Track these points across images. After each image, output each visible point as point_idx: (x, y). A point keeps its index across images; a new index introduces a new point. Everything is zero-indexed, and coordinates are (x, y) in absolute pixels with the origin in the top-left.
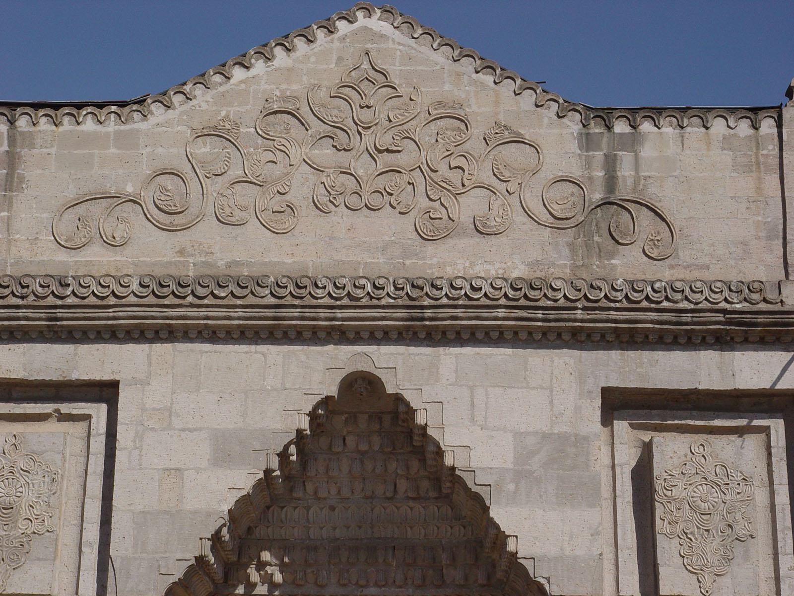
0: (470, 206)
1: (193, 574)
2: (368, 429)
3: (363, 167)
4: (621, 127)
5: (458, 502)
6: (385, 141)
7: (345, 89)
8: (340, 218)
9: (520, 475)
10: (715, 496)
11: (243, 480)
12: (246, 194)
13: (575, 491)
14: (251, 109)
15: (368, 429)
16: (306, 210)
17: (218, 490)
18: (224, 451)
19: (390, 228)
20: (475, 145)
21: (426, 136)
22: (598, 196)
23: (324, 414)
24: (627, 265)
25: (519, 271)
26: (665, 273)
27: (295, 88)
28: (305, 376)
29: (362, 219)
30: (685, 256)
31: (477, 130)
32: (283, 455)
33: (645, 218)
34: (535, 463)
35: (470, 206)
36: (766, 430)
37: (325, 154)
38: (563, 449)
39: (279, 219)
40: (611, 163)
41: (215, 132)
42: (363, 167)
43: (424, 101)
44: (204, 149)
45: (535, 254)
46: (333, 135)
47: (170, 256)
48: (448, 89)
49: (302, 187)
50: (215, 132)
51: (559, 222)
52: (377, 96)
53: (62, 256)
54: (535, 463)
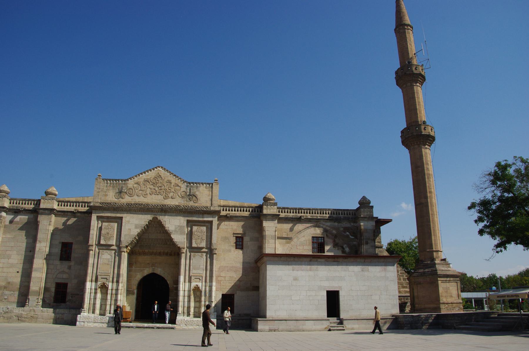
0: (171, 194)
1: (208, 284)
2: (156, 226)
3: (157, 189)
4: (192, 185)
5: (167, 234)
6: (160, 185)
7: (155, 178)
8: (153, 196)
9: (175, 231)
10: (200, 234)
11: (139, 230)
12: (140, 192)
13: (182, 233)
14: (142, 180)
15: (156, 226)
16: (149, 194)
17: (135, 232)
18: (136, 227)
19: (160, 197)
20: (172, 186)
21: (165, 185)
22: (188, 194)
23: (150, 222)
24: (191, 204)
25: (177, 204)
26: (196, 205)
27: (149, 177)
28: (149, 217)
29: (156, 196)
30: (199, 202)
31: (172, 184)
32: (144, 227)
33: (194, 198)
34: (177, 229)
35: (171, 194)
36: (211, 222)
37: (152, 187)
38: (181, 227)
39: (145, 196)
40: (190, 190)
41: (137, 183)
42: (157, 189)
43: (166, 180)
44: (135, 186)
45: (179, 201)
46: (153, 184)
47: (130, 200)
48: (170, 178)
49: (148, 191)
50: (137, 183)
51: (183, 197)
52: (159, 179)
53: (116, 200)
54: (177, 229)
